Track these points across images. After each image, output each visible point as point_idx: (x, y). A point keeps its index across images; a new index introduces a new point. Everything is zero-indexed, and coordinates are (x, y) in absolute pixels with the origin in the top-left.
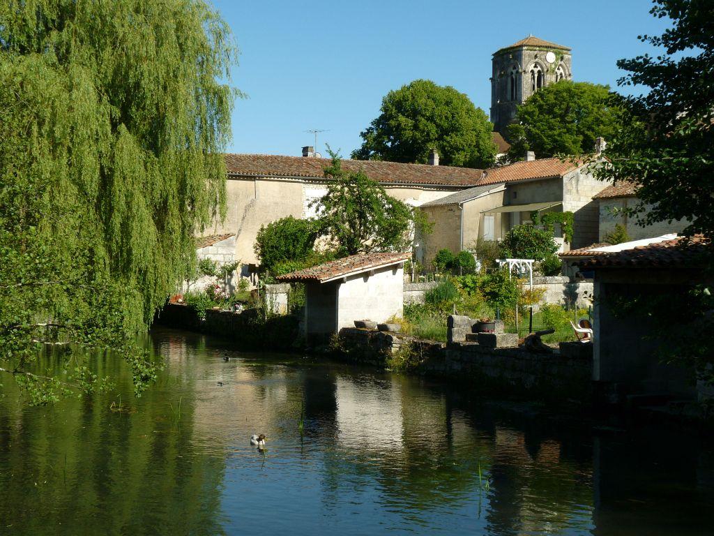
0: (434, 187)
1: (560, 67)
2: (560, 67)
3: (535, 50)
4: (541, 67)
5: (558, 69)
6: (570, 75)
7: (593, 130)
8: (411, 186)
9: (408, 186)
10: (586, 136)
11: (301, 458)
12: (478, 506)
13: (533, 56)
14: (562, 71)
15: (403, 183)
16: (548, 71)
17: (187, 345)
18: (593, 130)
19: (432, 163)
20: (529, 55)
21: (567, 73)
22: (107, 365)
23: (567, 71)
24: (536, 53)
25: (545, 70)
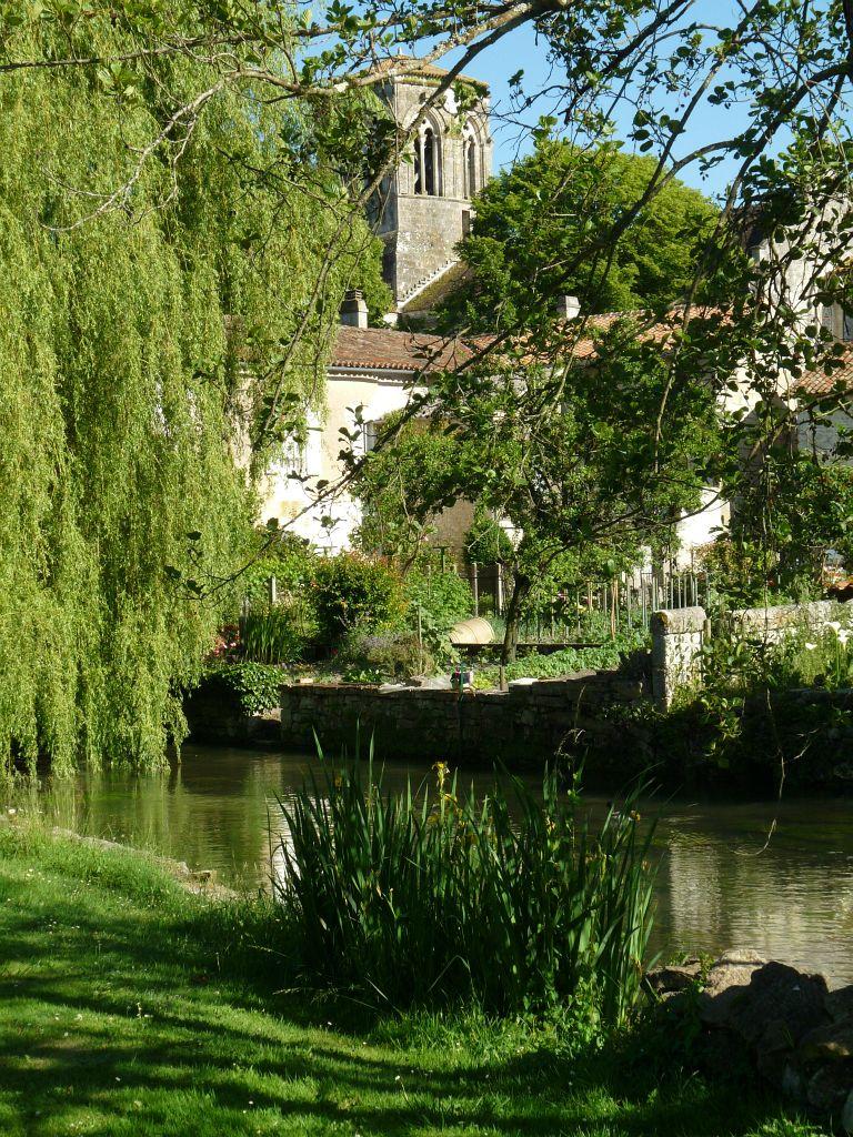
0: (381, 376)
1: (469, 124)
2: (469, 124)
3: (420, 84)
4: (434, 122)
5: (466, 128)
6: (489, 141)
7: (652, 253)
8: (355, 373)
9: (349, 373)
10: (640, 265)
11: (609, 606)
12: (837, 108)
13: (417, 97)
14: (471, 131)
15: (343, 368)
16: (447, 129)
17: (312, 641)
18: (652, 253)
19: (354, 323)
20: (409, 96)
21: (483, 137)
22: (93, 797)
23: (482, 132)
24: (421, 89)
25: (442, 128)
